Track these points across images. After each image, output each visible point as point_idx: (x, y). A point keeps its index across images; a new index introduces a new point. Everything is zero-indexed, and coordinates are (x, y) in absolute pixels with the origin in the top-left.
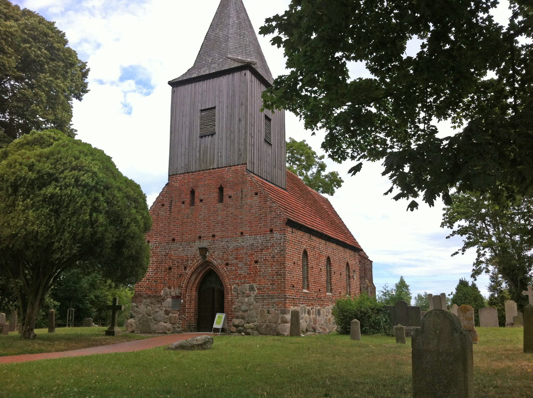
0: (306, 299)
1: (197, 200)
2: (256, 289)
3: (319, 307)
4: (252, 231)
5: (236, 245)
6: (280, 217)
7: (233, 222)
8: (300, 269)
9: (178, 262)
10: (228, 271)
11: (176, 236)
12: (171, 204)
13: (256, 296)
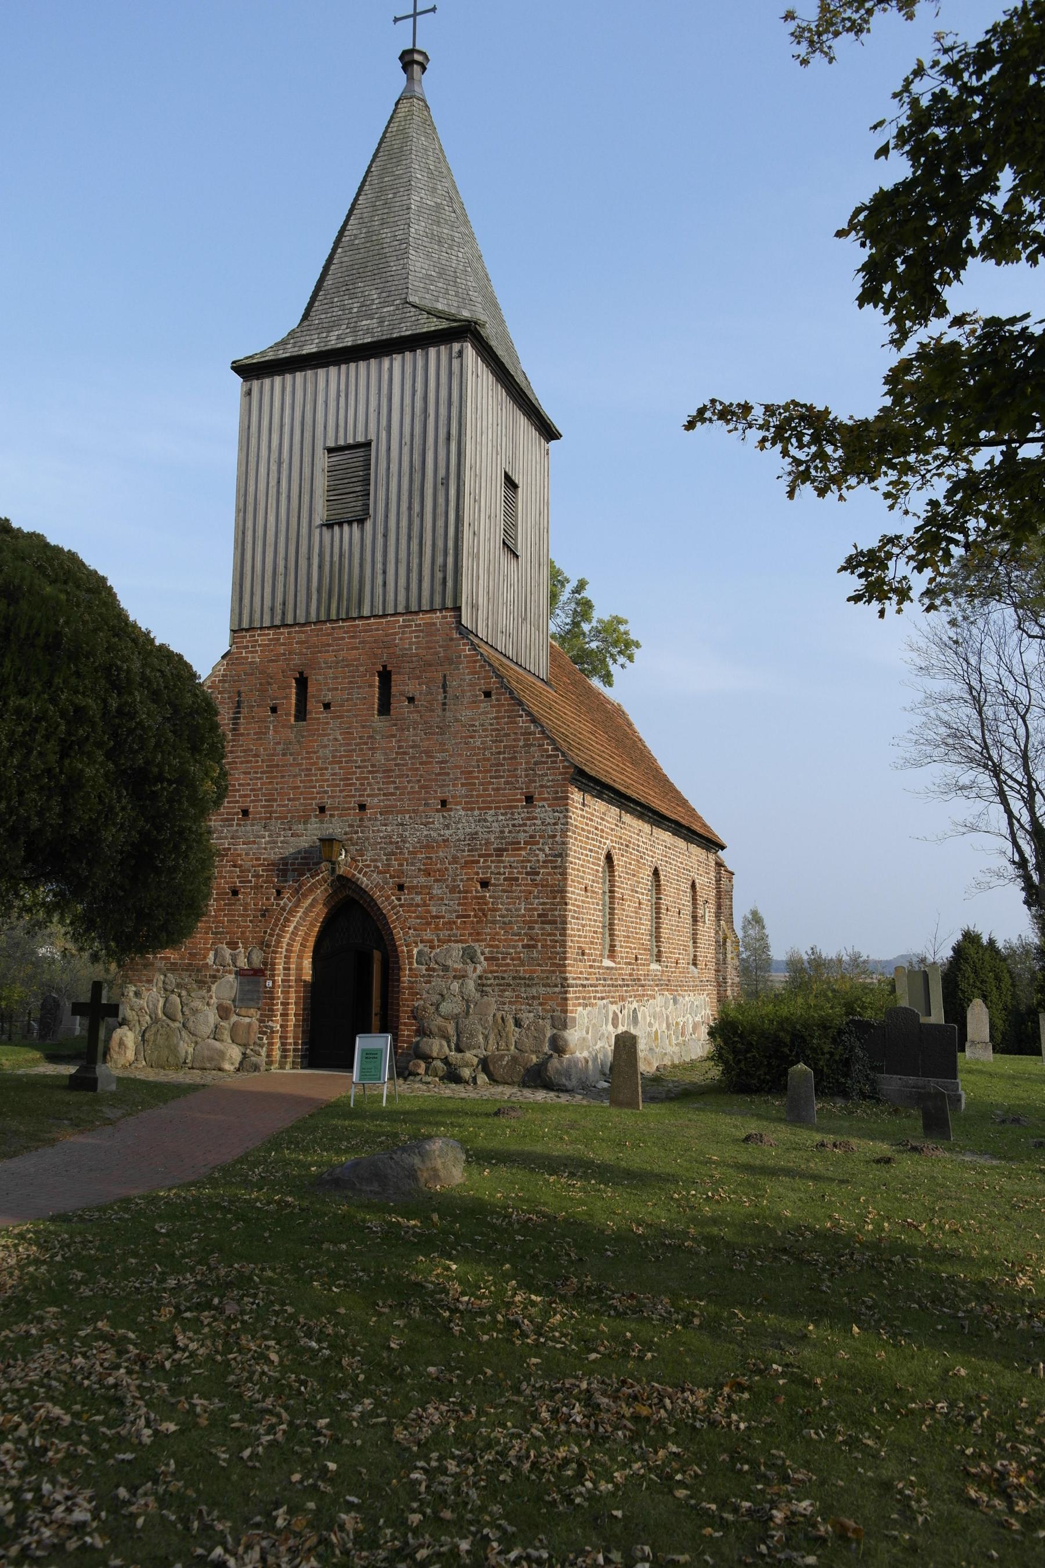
0: (609, 986)
1: (314, 707)
2: (482, 958)
3: (635, 1005)
4: (472, 796)
5: (426, 836)
6: (555, 762)
7: (417, 769)
8: (598, 904)
9: (257, 876)
10: (401, 906)
11: (252, 801)
12: (239, 713)
13: (480, 978)
